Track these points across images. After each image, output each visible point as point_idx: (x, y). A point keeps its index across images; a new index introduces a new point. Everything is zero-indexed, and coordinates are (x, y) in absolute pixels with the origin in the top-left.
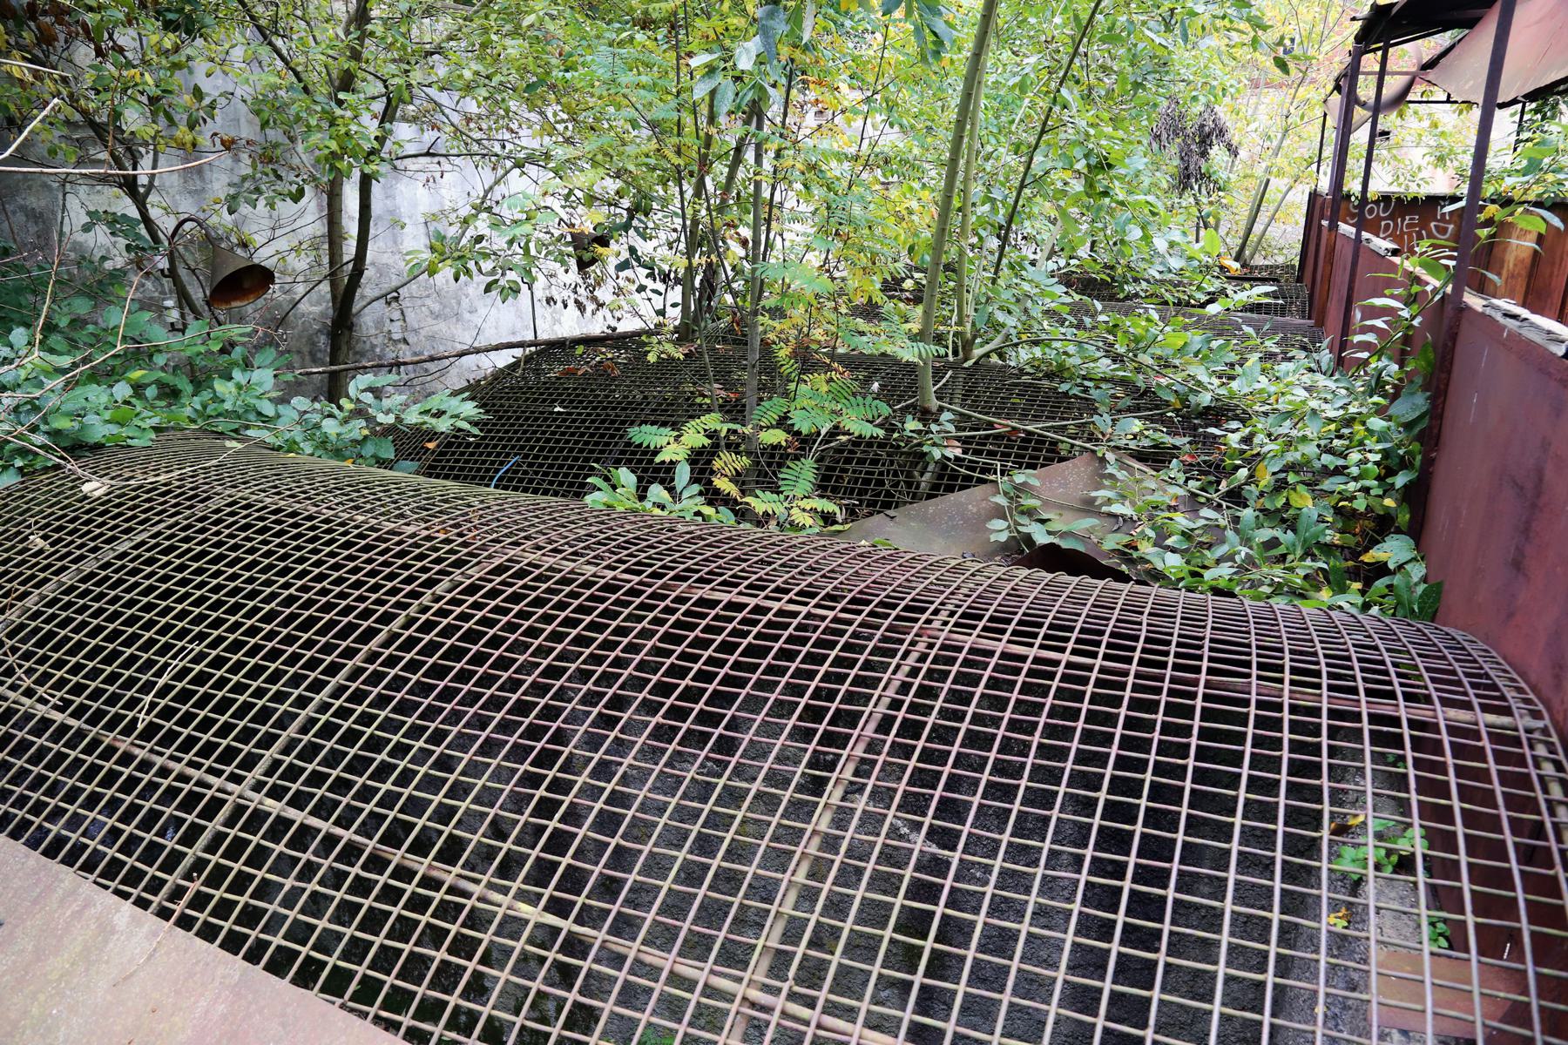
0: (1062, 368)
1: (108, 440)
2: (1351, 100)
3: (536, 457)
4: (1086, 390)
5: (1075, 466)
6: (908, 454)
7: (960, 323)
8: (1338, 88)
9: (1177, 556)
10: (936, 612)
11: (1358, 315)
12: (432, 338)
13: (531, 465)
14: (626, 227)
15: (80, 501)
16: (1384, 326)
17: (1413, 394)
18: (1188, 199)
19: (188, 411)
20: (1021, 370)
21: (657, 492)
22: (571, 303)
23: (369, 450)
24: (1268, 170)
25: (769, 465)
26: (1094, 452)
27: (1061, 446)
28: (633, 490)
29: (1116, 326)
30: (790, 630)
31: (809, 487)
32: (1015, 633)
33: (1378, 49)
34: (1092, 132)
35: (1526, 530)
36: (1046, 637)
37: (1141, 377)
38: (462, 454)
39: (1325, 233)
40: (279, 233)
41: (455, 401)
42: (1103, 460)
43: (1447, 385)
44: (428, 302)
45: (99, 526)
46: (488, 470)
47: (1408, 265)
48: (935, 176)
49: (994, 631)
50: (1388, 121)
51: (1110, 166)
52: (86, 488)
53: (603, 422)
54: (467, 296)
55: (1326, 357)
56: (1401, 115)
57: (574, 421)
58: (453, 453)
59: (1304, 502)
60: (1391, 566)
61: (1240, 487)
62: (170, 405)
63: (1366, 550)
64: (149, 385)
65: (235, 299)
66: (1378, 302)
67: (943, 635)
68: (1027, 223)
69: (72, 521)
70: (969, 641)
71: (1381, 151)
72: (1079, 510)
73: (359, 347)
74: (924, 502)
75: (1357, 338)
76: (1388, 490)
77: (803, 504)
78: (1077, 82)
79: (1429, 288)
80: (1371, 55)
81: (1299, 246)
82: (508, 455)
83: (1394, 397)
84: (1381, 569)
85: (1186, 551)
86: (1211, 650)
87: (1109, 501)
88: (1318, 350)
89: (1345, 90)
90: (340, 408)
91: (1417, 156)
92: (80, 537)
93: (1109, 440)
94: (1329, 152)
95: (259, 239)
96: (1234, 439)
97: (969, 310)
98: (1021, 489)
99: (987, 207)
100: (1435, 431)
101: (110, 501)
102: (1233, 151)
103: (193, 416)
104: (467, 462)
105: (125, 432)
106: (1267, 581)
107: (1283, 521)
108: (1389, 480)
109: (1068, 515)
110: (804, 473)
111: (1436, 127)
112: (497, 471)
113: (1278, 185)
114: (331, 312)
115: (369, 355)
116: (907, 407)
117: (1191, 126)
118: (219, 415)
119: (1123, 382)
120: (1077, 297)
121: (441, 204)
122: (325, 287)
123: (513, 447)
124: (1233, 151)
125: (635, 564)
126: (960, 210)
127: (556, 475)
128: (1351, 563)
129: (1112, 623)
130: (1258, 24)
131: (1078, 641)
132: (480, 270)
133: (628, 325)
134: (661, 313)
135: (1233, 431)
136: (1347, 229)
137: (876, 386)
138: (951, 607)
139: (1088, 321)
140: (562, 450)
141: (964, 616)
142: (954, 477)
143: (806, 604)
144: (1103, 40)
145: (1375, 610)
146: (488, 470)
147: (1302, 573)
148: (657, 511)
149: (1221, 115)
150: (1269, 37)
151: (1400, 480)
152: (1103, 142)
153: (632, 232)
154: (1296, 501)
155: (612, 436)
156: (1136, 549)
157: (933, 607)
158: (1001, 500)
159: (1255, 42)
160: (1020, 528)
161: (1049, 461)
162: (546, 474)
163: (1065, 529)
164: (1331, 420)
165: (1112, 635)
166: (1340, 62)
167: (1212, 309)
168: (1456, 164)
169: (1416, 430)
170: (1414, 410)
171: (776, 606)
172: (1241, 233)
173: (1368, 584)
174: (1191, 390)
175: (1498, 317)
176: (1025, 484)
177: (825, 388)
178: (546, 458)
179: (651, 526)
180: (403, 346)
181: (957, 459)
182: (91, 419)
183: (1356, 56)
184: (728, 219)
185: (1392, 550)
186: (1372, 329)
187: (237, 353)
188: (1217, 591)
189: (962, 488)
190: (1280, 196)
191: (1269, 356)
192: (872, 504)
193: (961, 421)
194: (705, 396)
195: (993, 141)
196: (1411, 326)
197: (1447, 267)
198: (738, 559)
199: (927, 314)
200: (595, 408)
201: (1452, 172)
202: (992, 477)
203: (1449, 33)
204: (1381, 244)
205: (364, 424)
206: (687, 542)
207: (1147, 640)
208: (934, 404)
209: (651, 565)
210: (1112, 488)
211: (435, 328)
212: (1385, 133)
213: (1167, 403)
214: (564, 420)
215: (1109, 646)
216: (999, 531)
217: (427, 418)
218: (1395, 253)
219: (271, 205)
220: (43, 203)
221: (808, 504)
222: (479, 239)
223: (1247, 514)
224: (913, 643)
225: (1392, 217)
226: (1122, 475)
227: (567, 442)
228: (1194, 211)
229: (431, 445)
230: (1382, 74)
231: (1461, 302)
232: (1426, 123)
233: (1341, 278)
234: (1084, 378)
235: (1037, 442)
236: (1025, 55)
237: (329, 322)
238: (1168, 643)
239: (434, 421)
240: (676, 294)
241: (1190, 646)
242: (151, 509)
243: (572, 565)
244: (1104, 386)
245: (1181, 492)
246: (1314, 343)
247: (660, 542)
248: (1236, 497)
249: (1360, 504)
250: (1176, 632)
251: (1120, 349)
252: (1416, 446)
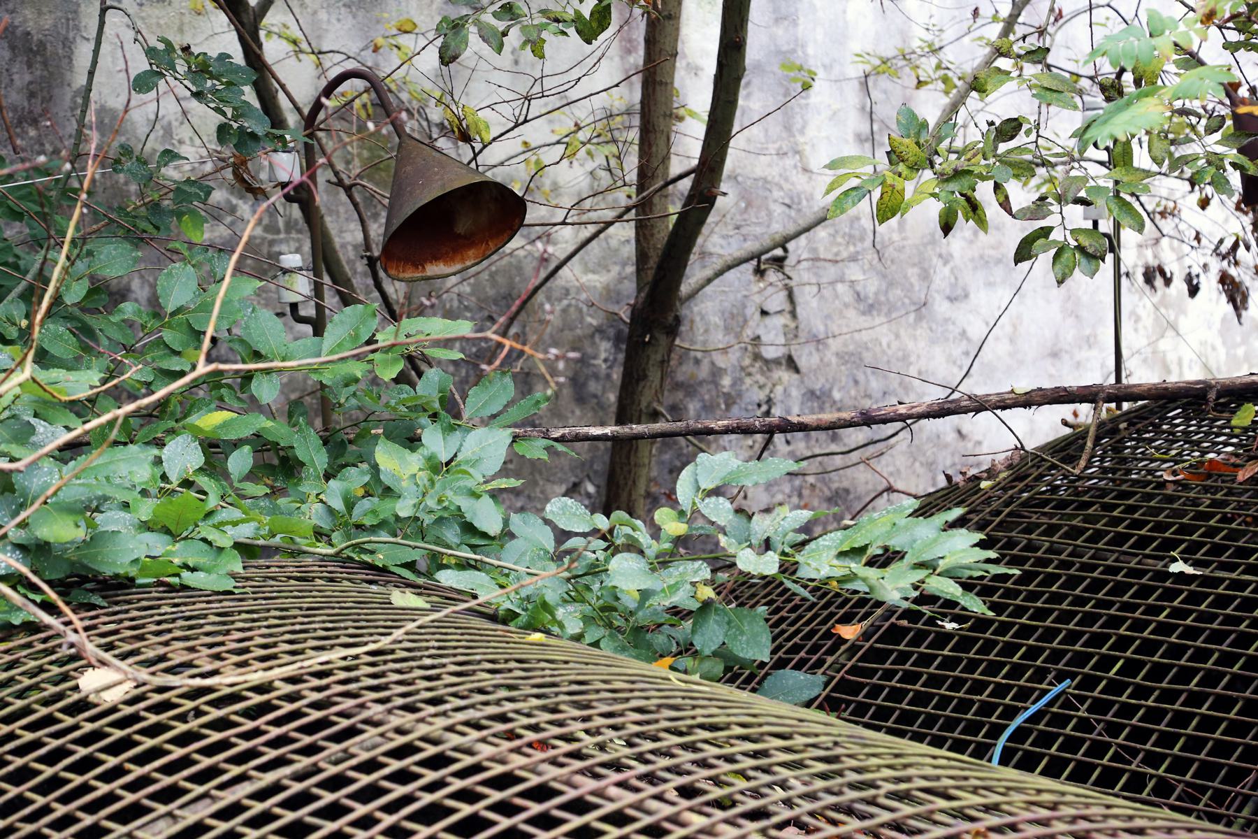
1: (144, 570)
3: (1115, 687)
12: (851, 358)
13: (1099, 707)
15: (72, 710)
19: (314, 514)
23: (710, 637)
38: (925, 660)
40: (537, 107)
41: (927, 529)
44: (854, 272)
45: (107, 777)
46: (987, 709)
52: (89, 681)
54: (946, 259)
57: (1222, 602)
58: (903, 657)
62: (275, 492)
64: (236, 444)
65: (435, 258)
69: (51, 759)
73: (683, 372)
82: (1040, 675)
90: (656, 532)
92: (64, 800)
95: (494, 122)
101: (134, 718)
103: (325, 525)
104: (935, 681)
105: (179, 553)
112: (1010, 713)
114: (630, 287)
115: (706, 393)
118: (382, 525)
121: (904, 35)
122: (624, 233)
123: (1056, 656)
132: (1005, 205)
146: (987, 709)
162: (1139, 735)
178: (1142, 693)
180: (784, 375)
182: (111, 520)
187: (431, 384)
205: (706, 573)
211: (865, 336)
214: (1195, 598)
217: (856, 566)
219: (537, 47)
220: (47, 22)
222: (1010, 128)
227: (1201, 655)
229: (849, 632)
237: (625, 314)
239: (873, 573)
242: (224, 745)
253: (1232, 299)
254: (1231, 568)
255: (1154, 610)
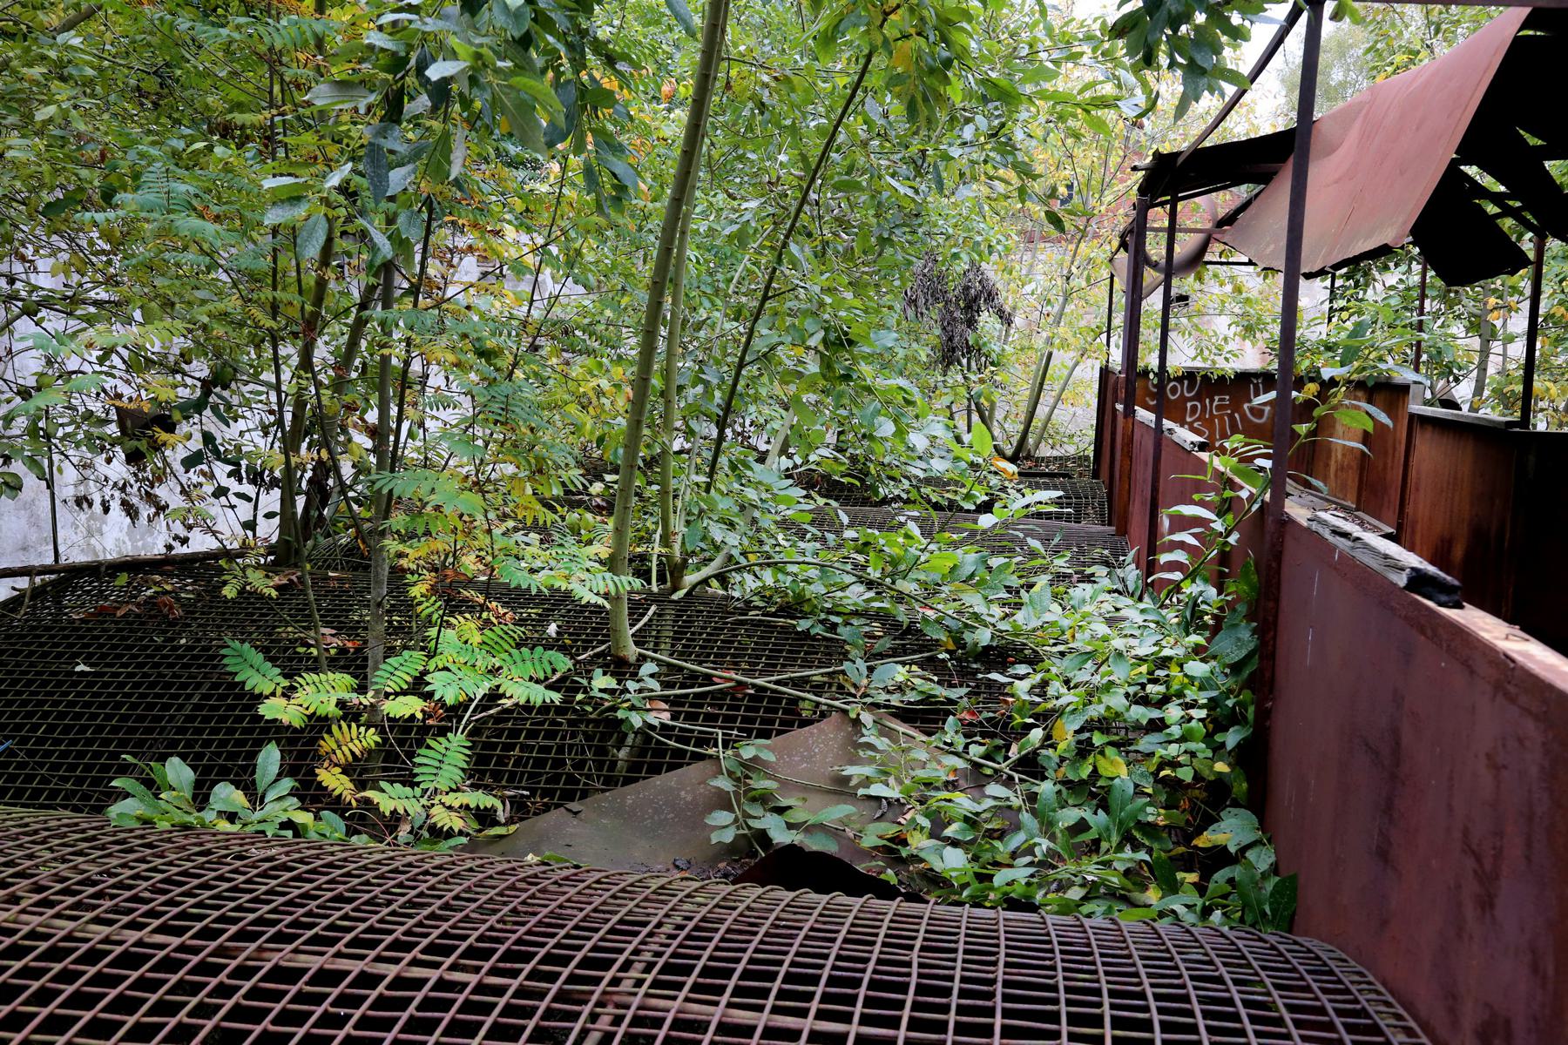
0: (801, 599)
2: (1140, 260)
3: (40, 741)
4: (833, 627)
5: (821, 731)
6: (596, 722)
7: (666, 541)
8: (1123, 245)
9: (959, 851)
10: (627, 966)
11: (1166, 523)
13: (31, 753)
14: (199, 406)
16: (1193, 541)
17: (1235, 626)
18: (955, 376)
20: (748, 602)
21: (227, 795)
22: (115, 506)
24: (1049, 341)
25: (401, 743)
26: (845, 712)
27: (801, 705)
28: (188, 794)
29: (867, 544)
30: (411, 1009)
31: (457, 775)
32: (738, 991)
33: (1166, 202)
34: (828, 300)
35: (1388, 808)
36: (782, 994)
37: (902, 608)
39: (1120, 418)
42: (857, 722)
43: (1276, 616)
47: (1218, 463)
48: (631, 346)
49: (707, 990)
50: (1184, 284)
51: (851, 343)
53: (152, 685)
55: (1131, 574)
56: (1200, 279)
57: (106, 685)
59: (1115, 768)
60: (1232, 849)
61: (1035, 753)
63: (1199, 831)
66: (1188, 510)
67: (636, 1001)
68: (752, 408)
70: (673, 1007)
71: (1179, 319)
72: (829, 792)
74: (620, 790)
75: (1164, 558)
76: (1217, 749)
77: (449, 799)
78: (809, 235)
79: (1244, 494)
80: (1159, 209)
81: (1092, 434)
83: (1216, 630)
84: (1220, 857)
85: (972, 842)
86: (1006, 998)
87: (867, 781)
88: (1121, 565)
89: (1131, 248)
91: (1222, 325)
93: (865, 695)
94: (1119, 320)
96: (1022, 687)
97: (678, 524)
98: (752, 766)
99: (700, 389)
100: (1268, 675)
102: (1006, 318)
106: (1078, 880)
107: (1093, 795)
108: (1219, 738)
109: (815, 800)
110: (452, 752)
111: (1240, 292)
113: (1062, 359)
116: (597, 655)
117: (953, 288)
119: (882, 617)
120: (821, 501)
124: (1006, 318)
125: (176, 917)
126: (662, 394)
127: (72, 768)
128: (1182, 849)
129: (871, 966)
130: (1025, 171)
131: (826, 998)
133: (201, 543)
134: (250, 525)
135: (1021, 678)
136: (1144, 415)
137: (552, 629)
138: (647, 957)
139: (830, 537)
140: (84, 729)
141: (667, 969)
142: (661, 750)
143: (437, 965)
144: (837, 188)
145: (1217, 916)
147: (1121, 867)
148: (224, 826)
149: (990, 274)
150: (1038, 187)
151: (1231, 738)
152: (842, 314)
153: (208, 412)
154: (1105, 768)
155: (166, 707)
156: (905, 843)
157: (622, 958)
158: (724, 783)
159: (1023, 193)
160: (751, 822)
161: (787, 726)
163: (812, 820)
164: (1142, 660)
165: (873, 985)
166: (1123, 217)
167: (986, 521)
168: (1266, 335)
169: (1246, 673)
170: (1240, 648)
171: (391, 971)
172: (1022, 417)
173: (1206, 876)
174: (966, 625)
175: (1327, 534)
176: (755, 759)
177: (476, 638)
178: (57, 742)
179: (208, 853)
181: (664, 726)
183: (1142, 210)
184: (347, 399)
185: (1230, 830)
186: (1182, 545)
188: (1012, 904)
189: (672, 767)
190: (1066, 373)
191: (1060, 577)
192: (546, 793)
193: (668, 675)
194: (309, 646)
195: (707, 304)
196: (1226, 543)
197: (1262, 469)
198: (339, 898)
199: (619, 531)
200: (140, 666)
201: (1261, 345)
202: (712, 751)
203: (1244, 187)
204: (1185, 436)
206: (264, 875)
207: (921, 990)
208: (631, 651)
209: (201, 918)
210: (871, 761)
212: (1183, 298)
213: (937, 643)
214: (90, 685)
215: (869, 1002)
216: (723, 827)
218: (1203, 447)
221: (455, 800)
223: (1046, 788)
224: (594, 1017)
225: (1198, 397)
226: (882, 743)
227: (94, 716)
228: (963, 392)
230: (1172, 231)
231: (1283, 513)
232: (1229, 288)
233: (1143, 474)
234: (829, 612)
235: (771, 700)
236: (744, 199)
238: (947, 992)
240: (271, 500)
241: (979, 990)
243: (70, 925)
244: (855, 622)
245: (960, 764)
246: (1116, 556)
247: (221, 878)
248: (1031, 766)
249: (1186, 774)
250: (958, 974)
251: (874, 573)
252: (1246, 695)
253: (129, 514)
254: (111, 665)
255: (67, 694)
